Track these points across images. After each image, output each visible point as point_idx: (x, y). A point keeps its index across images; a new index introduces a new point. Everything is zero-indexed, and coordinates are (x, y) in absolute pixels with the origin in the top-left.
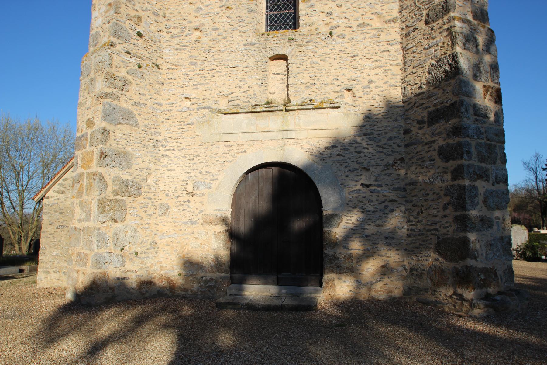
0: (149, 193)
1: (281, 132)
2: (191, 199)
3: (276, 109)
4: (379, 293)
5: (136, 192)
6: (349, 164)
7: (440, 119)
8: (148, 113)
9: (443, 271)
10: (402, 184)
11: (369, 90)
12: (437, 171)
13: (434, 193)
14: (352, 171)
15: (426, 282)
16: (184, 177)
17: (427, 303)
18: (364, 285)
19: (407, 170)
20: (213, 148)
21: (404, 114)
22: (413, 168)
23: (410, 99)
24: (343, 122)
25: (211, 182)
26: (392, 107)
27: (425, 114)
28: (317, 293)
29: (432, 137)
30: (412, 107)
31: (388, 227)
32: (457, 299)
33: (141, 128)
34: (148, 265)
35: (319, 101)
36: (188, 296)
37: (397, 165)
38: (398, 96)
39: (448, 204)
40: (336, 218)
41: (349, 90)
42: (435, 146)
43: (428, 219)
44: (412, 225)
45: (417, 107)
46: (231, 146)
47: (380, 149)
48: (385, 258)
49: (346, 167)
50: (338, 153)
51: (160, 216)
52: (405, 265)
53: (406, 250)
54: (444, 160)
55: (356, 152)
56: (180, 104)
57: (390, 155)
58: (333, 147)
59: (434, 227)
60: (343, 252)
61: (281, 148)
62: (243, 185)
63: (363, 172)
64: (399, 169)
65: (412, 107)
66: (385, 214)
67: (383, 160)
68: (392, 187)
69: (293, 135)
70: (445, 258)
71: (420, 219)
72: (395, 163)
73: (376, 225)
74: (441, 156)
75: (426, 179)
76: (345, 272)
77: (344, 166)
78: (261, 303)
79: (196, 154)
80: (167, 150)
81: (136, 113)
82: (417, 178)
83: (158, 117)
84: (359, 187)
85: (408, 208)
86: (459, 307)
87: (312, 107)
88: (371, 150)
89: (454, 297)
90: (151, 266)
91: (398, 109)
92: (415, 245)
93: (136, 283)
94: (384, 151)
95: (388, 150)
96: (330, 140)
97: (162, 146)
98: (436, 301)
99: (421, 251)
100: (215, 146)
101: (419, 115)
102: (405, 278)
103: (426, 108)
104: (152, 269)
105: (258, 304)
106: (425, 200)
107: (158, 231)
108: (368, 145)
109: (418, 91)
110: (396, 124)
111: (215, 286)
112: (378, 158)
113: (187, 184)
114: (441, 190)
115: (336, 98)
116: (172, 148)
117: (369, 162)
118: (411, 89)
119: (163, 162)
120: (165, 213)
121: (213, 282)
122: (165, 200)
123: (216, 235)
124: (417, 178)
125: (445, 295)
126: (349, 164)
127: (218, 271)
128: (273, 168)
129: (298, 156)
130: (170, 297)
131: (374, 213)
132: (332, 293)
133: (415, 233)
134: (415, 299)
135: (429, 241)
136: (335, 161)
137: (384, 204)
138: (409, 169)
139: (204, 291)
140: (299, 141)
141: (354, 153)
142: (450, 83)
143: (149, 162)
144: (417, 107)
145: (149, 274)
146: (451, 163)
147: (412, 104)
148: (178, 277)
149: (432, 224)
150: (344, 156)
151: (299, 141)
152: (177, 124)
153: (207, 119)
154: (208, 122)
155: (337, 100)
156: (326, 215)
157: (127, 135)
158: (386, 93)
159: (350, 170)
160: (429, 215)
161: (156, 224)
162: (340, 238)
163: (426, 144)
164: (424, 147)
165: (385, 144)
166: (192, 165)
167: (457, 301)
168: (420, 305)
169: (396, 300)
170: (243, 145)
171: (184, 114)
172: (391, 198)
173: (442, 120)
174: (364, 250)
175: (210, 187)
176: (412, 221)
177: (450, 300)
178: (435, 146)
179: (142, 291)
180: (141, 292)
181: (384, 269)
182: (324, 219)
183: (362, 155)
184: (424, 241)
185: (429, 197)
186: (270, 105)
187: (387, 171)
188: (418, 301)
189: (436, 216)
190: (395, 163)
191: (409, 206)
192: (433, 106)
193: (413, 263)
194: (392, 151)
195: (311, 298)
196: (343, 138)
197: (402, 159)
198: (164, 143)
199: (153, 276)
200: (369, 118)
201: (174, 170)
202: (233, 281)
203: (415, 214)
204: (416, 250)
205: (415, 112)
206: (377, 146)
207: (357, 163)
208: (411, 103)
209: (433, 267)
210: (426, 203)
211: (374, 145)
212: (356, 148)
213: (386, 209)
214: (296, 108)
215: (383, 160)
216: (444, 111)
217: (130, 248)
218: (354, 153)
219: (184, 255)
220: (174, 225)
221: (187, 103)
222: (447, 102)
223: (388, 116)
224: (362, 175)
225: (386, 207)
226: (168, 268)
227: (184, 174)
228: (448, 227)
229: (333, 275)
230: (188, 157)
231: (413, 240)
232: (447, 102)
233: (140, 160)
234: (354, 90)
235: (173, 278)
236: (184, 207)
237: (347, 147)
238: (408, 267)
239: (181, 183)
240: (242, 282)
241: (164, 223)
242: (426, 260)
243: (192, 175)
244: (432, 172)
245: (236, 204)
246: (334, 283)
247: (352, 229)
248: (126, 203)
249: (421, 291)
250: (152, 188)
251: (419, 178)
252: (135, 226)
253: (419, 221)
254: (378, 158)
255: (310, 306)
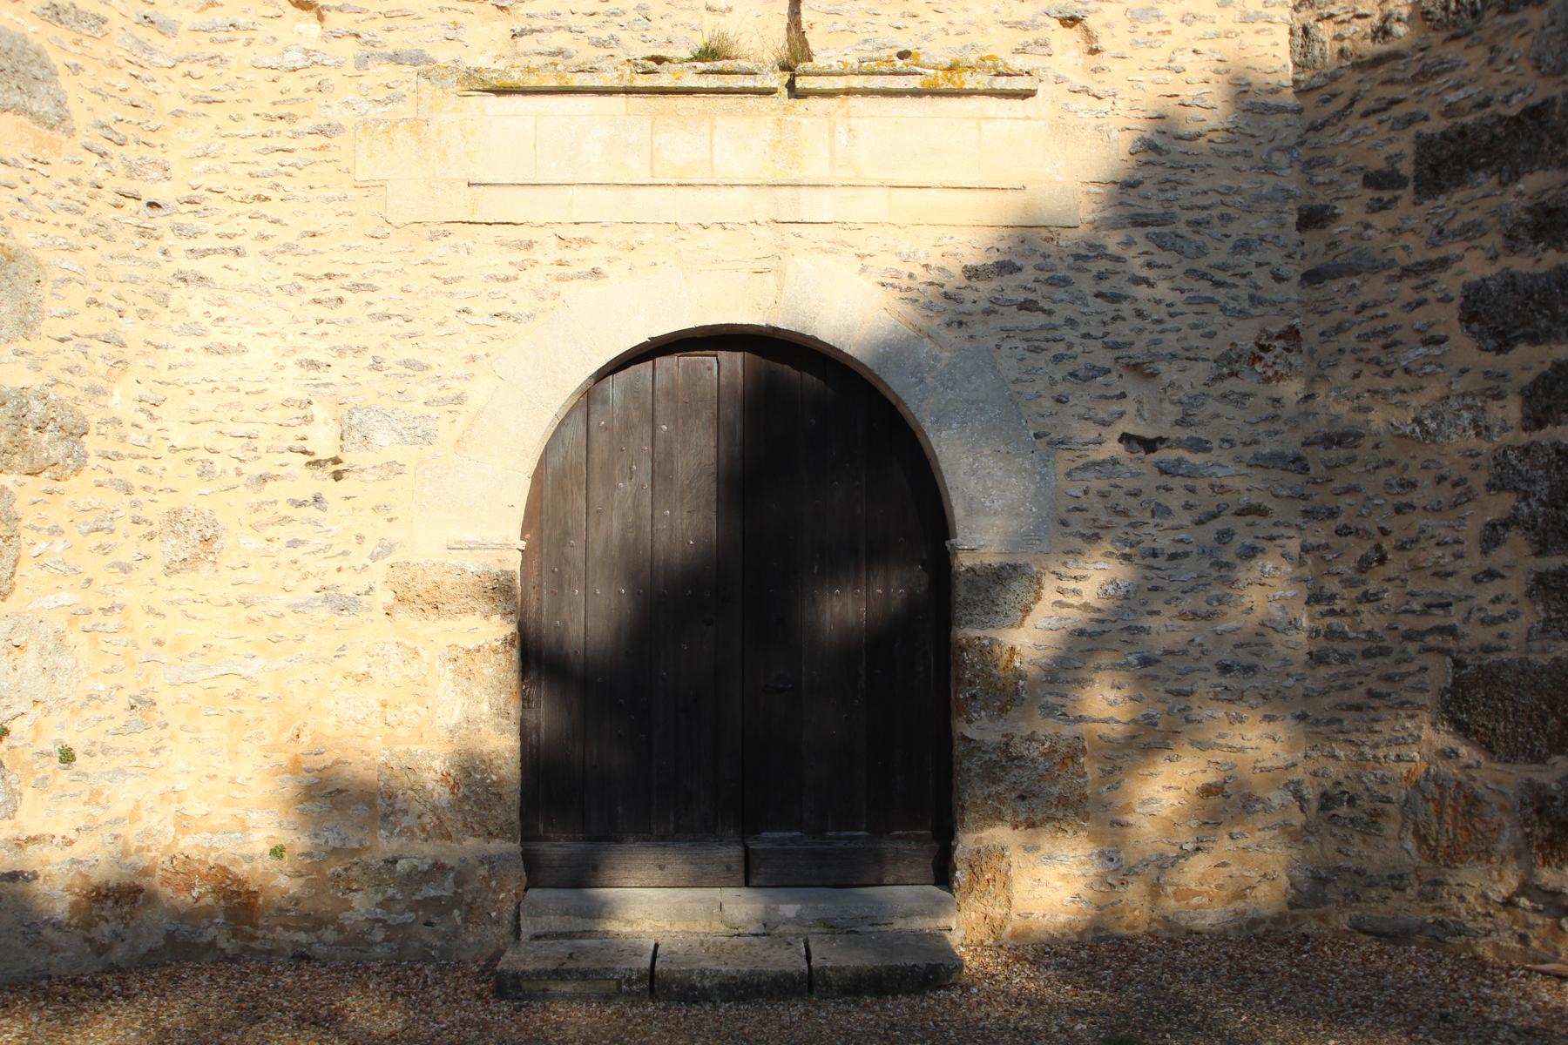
0: (118, 456)
1: (766, 191)
2: (330, 489)
3: (748, 82)
4: (1195, 901)
5: (58, 452)
6: (1070, 346)
7: (1475, 169)
8: (113, 64)
9: (1474, 801)
10: (1290, 442)
11: (1156, 27)
12: (1458, 387)
13: (1441, 479)
14: (1085, 380)
15: (1396, 847)
16: (292, 383)
17: (1396, 935)
18: (1132, 871)
19: (1311, 381)
20: (440, 249)
21: (1301, 144)
22: (1342, 373)
23: (1333, 78)
24: (1051, 159)
25: (432, 411)
26: (1252, 109)
27: (1404, 144)
28: (934, 915)
29: (1435, 245)
30: (1341, 115)
31: (1233, 624)
32: (1536, 910)
33: (81, 138)
34: (120, 808)
35: (946, 61)
36: (321, 950)
37: (1269, 357)
38: (1277, 65)
39: (1505, 525)
40: (1015, 585)
41: (1070, 21)
42: (1450, 282)
43: (1409, 588)
44: (1332, 612)
45: (1365, 115)
46: (530, 245)
47: (1204, 289)
48: (1219, 756)
49: (1058, 359)
50: (1021, 296)
51: (169, 570)
52: (1299, 783)
53: (1302, 717)
54: (1491, 343)
55: (1099, 295)
56: (267, 29)
57: (1242, 314)
58: (1005, 267)
59: (1438, 618)
60: (1041, 732)
61: (766, 264)
62: (577, 429)
63: (1129, 384)
64: (1279, 377)
65: (1341, 115)
66: (1221, 565)
67: (1211, 335)
68: (1248, 453)
69: (821, 205)
70: (1488, 748)
71: (1372, 587)
72: (1263, 348)
73: (1182, 615)
74: (1475, 326)
75: (1404, 420)
76: (1052, 819)
77: (1049, 355)
78: (711, 965)
79: (356, 277)
80: (205, 253)
81: (56, 58)
82: (1359, 418)
83: (158, 87)
84: (1113, 448)
85: (1312, 541)
86: (1543, 944)
87: (914, 83)
88: (1162, 290)
89: (1524, 902)
90: (134, 816)
91: (1278, 121)
92: (1346, 697)
93: (70, 898)
94: (1220, 294)
95: (1234, 291)
96: (985, 237)
97: (178, 230)
98: (1442, 924)
99: (1376, 720)
100: (451, 240)
101: (1374, 147)
102: (1297, 836)
103: (1410, 120)
104: (139, 827)
105: (702, 973)
106: (1399, 510)
107: (159, 643)
108: (1150, 265)
109: (1371, 48)
110: (1270, 182)
111: (456, 901)
112: (1195, 327)
113: (308, 420)
114: (1475, 468)
115: (1017, 52)
116: (227, 243)
117: (1156, 342)
118: (1339, 38)
119: (185, 311)
120: (196, 558)
121: (449, 882)
122: (193, 496)
123: (462, 661)
124: (1359, 418)
125: (1484, 896)
126: (1070, 346)
127: (469, 829)
128: (724, 355)
129: (846, 305)
130: (233, 960)
131: (1185, 560)
132: (998, 912)
133: (1345, 647)
134: (1342, 921)
135: (1411, 681)
136: (1008, 333)
137: (1216, 525)
138: (1323, 377)
139: (403, 926)
140: (848, 236)
141: (1090, 300)
142: (1522, 24)
143: (118, 305)
144: (1365, 115)
145: (125, 853)
146: (1522, 351)
147: (1341, 102)
148: (270, 863)
149: (1429, 606)
150: (1049, 313)
151: (848, 240)
152: (254, 126)
153: (406, 109)
154: (416, 126)
155: (1018, 63)
156: (971, 570)
157: (16, 164)
158: (1227, 48)
159: (1073, 375)
160: (1417, 568)
161: (150, 611)
162: (1033, 672)
163: (1407, 272)
164: (1395, 286)
165: (1223, 267)
166: (331, 329)
167: (1534, 919)
168: (1368, 945)
169: (1261, 930)
170: (584, 241)
171: (288, 80)
172: (1244, 499)
173: (1481, 177)
174: (1134, 721)
175: (426, 437)
176: (1333, 597)
177: (1503, 915)
178: (1450, 282)
179: (94, 933)
180: (90, 941)
181: (1213, 800)
182: (961, 591)
183: (1126, 308)
184: (1389, 678)
185: (1414, 497)
186: (719, 65)
187: (1230, 385)
188: (1358, 927)
189: (1450, 574)
190: (1263, 348)
191: (1321, 533)
192: (1444, 114)
193: (1333, 769)
194: (1252, 297)
195: (920, 936)
196: (1044, 233)
197: (1291, 335)
198: (187, 218)
199: (144, 861)
200: (1161, 149)
201: (241, 349)
202: (535, 872)
203: (1347, 567)
204: (1348, 719)
205: (1356, 134)
206: (1190, 272)
207: (1106, 346)
208: (1334, 96)
209: (1432, 786)
210: (1402, 520)
211: (1178, 270)
212: (1100, 277)
213: (1224, 546)
214: (840, 83)
215: (1211, 335)
216: (1494, 137)
217: (37, 727)
218: (1090, 300)
219: (296, 761)
220: (243, 613)
221: (302, 26)
222: (1506, 101)
223: (1234, 148)
224: (1123, 395)
225: (1225, 536)
226: (216, 821)
227: (292, 371)
228: (1502, 619)
229: (1000, 834)
230: (314, 290)
231: (1336, 676)
232: (1506, 101)
233: (76, 296)
234: (1091, 22)
235: (242, 870)
236: (296, 530)
237: (1062, 272)
238: (1310, 793)
239: (278, 414)
240: (583, 875)
241: (191, 608)
242: (1399, 758)
243: (333, 376)
244: (1434, 390)
245: (545, 514)
246: (1003, 866)
247: (1081, 633)
248: (17, 507)
249: (1371, 885)
250: (135, 436)
251: (1371, 415)
252: (60, 621)
253: (1366, 598)
254: (1195, 327)
255: (934, 972)
